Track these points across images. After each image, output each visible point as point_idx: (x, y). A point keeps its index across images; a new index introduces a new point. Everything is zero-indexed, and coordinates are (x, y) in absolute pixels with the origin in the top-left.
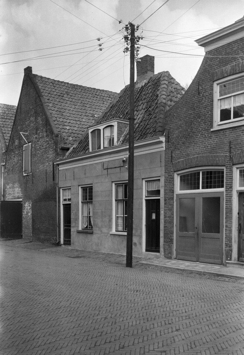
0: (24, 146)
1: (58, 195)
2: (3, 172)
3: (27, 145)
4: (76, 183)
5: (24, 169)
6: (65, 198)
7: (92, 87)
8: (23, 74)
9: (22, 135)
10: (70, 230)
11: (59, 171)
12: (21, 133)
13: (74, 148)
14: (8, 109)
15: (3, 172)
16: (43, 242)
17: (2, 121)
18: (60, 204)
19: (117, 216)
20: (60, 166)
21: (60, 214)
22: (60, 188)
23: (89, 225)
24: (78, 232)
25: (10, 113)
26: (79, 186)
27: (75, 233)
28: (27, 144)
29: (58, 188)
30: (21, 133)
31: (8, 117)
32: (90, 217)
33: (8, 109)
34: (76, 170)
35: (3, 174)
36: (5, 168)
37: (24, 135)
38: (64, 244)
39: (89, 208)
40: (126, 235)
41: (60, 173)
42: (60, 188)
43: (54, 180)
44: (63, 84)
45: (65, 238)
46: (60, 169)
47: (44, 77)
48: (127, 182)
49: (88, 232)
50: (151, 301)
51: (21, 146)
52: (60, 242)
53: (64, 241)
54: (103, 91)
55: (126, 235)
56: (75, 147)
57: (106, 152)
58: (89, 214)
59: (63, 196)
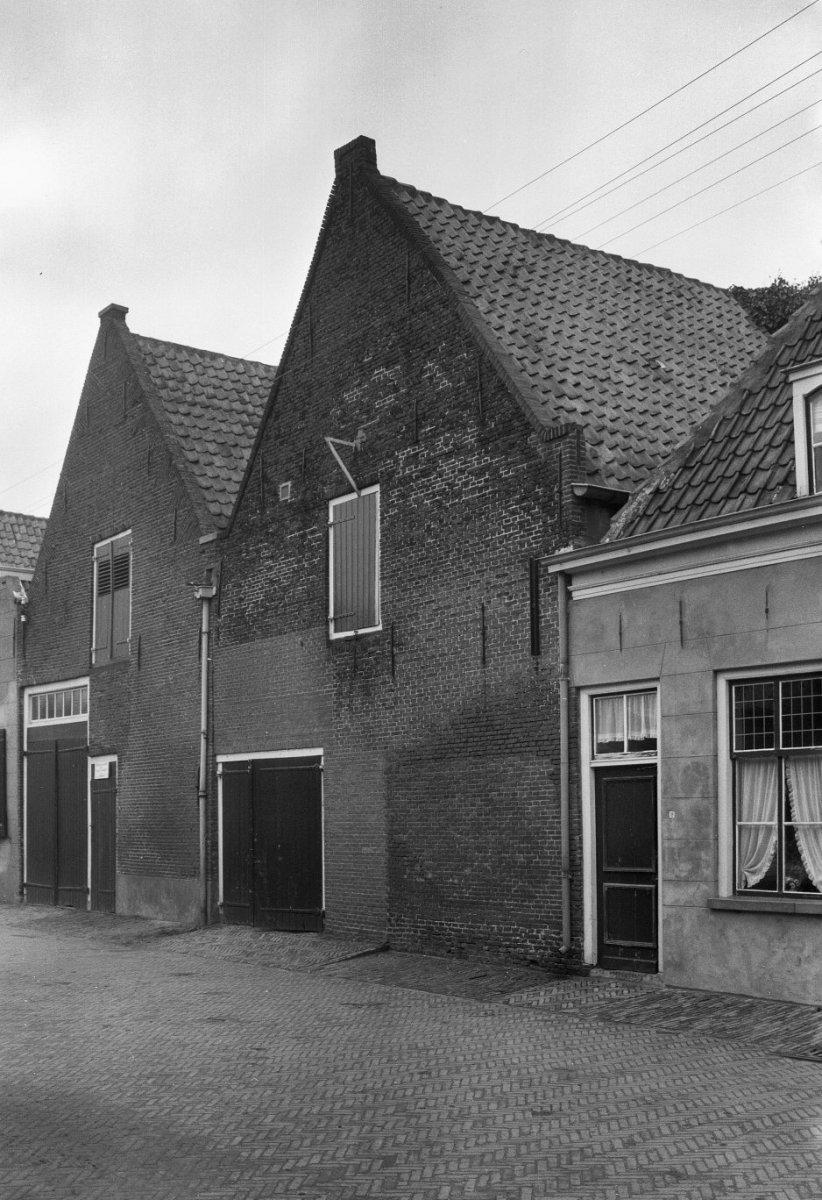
0: (333, 503)
1: (569, 720)
2: (205, 628)
3: (354, 496)
4: (695, 662)
5: (94, 644)
6: (606, 737)
7: (608, 250)
8: (334, 177)
9: (333, 449)
10: (650, 899)
11: (576, 612)
12: (329, 439)
13: (657, 492)
14: (194, 366)
15: (205, 628)
16: (462, 954)
17: (178, 412)
18: (579, 770)
19: (785, 823)
20: (577, 583)
21: (580, 817)
22: (579, 689)
23: (787, 875)
24: (715, 911)
25: (203, 380)
26: (716, 672)
27: (690, 918)
28: (351, 491)
29: (569, 690)
30: (329, 439)
31: (198, 399)
32: (791, 831)
33: (194, 366)
34: (691, 597)
35: (204, 638)
36: (216, 612)
37: (339, 447)
38: (602, 962)
39: (788, 792)
40: (819, 911)
41: (580, 616)
42: (579, 689)
43: (536, 650)
44: (184, 355)
45: (614, 935)
46: (576, 596)
47: (423, 194)
48: (818, 668)
49: (799, 910)
50: (439, 1114)
51: (311, 509)
52: (576, 952)
53: (602, 948)
54: (650, 268)
55: (819, 911)
56: (663, 487)
57: (777, 522)
58: (789, 818)
59: (601, 736)
